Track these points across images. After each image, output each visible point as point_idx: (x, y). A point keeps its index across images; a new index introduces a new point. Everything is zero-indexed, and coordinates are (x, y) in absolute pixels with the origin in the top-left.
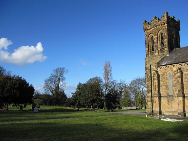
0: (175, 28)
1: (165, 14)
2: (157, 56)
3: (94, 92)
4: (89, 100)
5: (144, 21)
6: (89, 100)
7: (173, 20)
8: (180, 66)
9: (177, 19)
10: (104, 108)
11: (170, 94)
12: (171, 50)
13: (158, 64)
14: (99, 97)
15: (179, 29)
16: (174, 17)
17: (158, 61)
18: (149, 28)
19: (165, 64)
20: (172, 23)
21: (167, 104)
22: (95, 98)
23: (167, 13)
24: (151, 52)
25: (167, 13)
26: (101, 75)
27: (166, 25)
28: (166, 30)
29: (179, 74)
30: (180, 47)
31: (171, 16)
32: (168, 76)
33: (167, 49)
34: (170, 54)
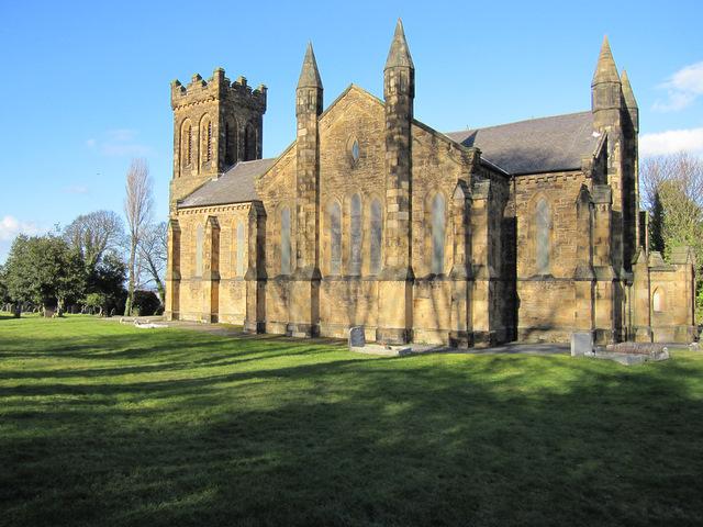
0: (248, 107)
1: (217, 74)
2: (195, 177)
3: (47, 265)
4: (32, 287)
5: (173, 81)
6: (32, 287)
7: (242, 88)
8: (213, 214)
9: (254, 85)
10: (126, 313)
11: (197, 275)
12: (226, 162)
13: (179, 202)
14: (61, 279)
15: (263, 109)
16: (245, 81)
17: (179, 198)
18: (183, 103)
19: (191, 204)
20: (235, 97)
21: (189, 298)
22: (49, 281)
23: (222, 73)
24: (185, 165)
25: (222, 73)
26: (114, 203)
27: (217, 101)
28: (217, 115)
29: (209, 231)
30: (260, 157)
31: (234, 77)
32: (195, 233)
33: (214, 164)
34: (219, 176)
